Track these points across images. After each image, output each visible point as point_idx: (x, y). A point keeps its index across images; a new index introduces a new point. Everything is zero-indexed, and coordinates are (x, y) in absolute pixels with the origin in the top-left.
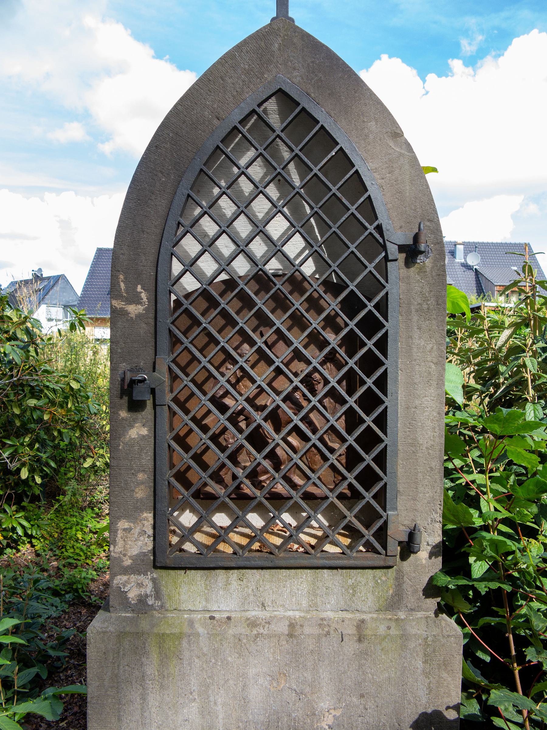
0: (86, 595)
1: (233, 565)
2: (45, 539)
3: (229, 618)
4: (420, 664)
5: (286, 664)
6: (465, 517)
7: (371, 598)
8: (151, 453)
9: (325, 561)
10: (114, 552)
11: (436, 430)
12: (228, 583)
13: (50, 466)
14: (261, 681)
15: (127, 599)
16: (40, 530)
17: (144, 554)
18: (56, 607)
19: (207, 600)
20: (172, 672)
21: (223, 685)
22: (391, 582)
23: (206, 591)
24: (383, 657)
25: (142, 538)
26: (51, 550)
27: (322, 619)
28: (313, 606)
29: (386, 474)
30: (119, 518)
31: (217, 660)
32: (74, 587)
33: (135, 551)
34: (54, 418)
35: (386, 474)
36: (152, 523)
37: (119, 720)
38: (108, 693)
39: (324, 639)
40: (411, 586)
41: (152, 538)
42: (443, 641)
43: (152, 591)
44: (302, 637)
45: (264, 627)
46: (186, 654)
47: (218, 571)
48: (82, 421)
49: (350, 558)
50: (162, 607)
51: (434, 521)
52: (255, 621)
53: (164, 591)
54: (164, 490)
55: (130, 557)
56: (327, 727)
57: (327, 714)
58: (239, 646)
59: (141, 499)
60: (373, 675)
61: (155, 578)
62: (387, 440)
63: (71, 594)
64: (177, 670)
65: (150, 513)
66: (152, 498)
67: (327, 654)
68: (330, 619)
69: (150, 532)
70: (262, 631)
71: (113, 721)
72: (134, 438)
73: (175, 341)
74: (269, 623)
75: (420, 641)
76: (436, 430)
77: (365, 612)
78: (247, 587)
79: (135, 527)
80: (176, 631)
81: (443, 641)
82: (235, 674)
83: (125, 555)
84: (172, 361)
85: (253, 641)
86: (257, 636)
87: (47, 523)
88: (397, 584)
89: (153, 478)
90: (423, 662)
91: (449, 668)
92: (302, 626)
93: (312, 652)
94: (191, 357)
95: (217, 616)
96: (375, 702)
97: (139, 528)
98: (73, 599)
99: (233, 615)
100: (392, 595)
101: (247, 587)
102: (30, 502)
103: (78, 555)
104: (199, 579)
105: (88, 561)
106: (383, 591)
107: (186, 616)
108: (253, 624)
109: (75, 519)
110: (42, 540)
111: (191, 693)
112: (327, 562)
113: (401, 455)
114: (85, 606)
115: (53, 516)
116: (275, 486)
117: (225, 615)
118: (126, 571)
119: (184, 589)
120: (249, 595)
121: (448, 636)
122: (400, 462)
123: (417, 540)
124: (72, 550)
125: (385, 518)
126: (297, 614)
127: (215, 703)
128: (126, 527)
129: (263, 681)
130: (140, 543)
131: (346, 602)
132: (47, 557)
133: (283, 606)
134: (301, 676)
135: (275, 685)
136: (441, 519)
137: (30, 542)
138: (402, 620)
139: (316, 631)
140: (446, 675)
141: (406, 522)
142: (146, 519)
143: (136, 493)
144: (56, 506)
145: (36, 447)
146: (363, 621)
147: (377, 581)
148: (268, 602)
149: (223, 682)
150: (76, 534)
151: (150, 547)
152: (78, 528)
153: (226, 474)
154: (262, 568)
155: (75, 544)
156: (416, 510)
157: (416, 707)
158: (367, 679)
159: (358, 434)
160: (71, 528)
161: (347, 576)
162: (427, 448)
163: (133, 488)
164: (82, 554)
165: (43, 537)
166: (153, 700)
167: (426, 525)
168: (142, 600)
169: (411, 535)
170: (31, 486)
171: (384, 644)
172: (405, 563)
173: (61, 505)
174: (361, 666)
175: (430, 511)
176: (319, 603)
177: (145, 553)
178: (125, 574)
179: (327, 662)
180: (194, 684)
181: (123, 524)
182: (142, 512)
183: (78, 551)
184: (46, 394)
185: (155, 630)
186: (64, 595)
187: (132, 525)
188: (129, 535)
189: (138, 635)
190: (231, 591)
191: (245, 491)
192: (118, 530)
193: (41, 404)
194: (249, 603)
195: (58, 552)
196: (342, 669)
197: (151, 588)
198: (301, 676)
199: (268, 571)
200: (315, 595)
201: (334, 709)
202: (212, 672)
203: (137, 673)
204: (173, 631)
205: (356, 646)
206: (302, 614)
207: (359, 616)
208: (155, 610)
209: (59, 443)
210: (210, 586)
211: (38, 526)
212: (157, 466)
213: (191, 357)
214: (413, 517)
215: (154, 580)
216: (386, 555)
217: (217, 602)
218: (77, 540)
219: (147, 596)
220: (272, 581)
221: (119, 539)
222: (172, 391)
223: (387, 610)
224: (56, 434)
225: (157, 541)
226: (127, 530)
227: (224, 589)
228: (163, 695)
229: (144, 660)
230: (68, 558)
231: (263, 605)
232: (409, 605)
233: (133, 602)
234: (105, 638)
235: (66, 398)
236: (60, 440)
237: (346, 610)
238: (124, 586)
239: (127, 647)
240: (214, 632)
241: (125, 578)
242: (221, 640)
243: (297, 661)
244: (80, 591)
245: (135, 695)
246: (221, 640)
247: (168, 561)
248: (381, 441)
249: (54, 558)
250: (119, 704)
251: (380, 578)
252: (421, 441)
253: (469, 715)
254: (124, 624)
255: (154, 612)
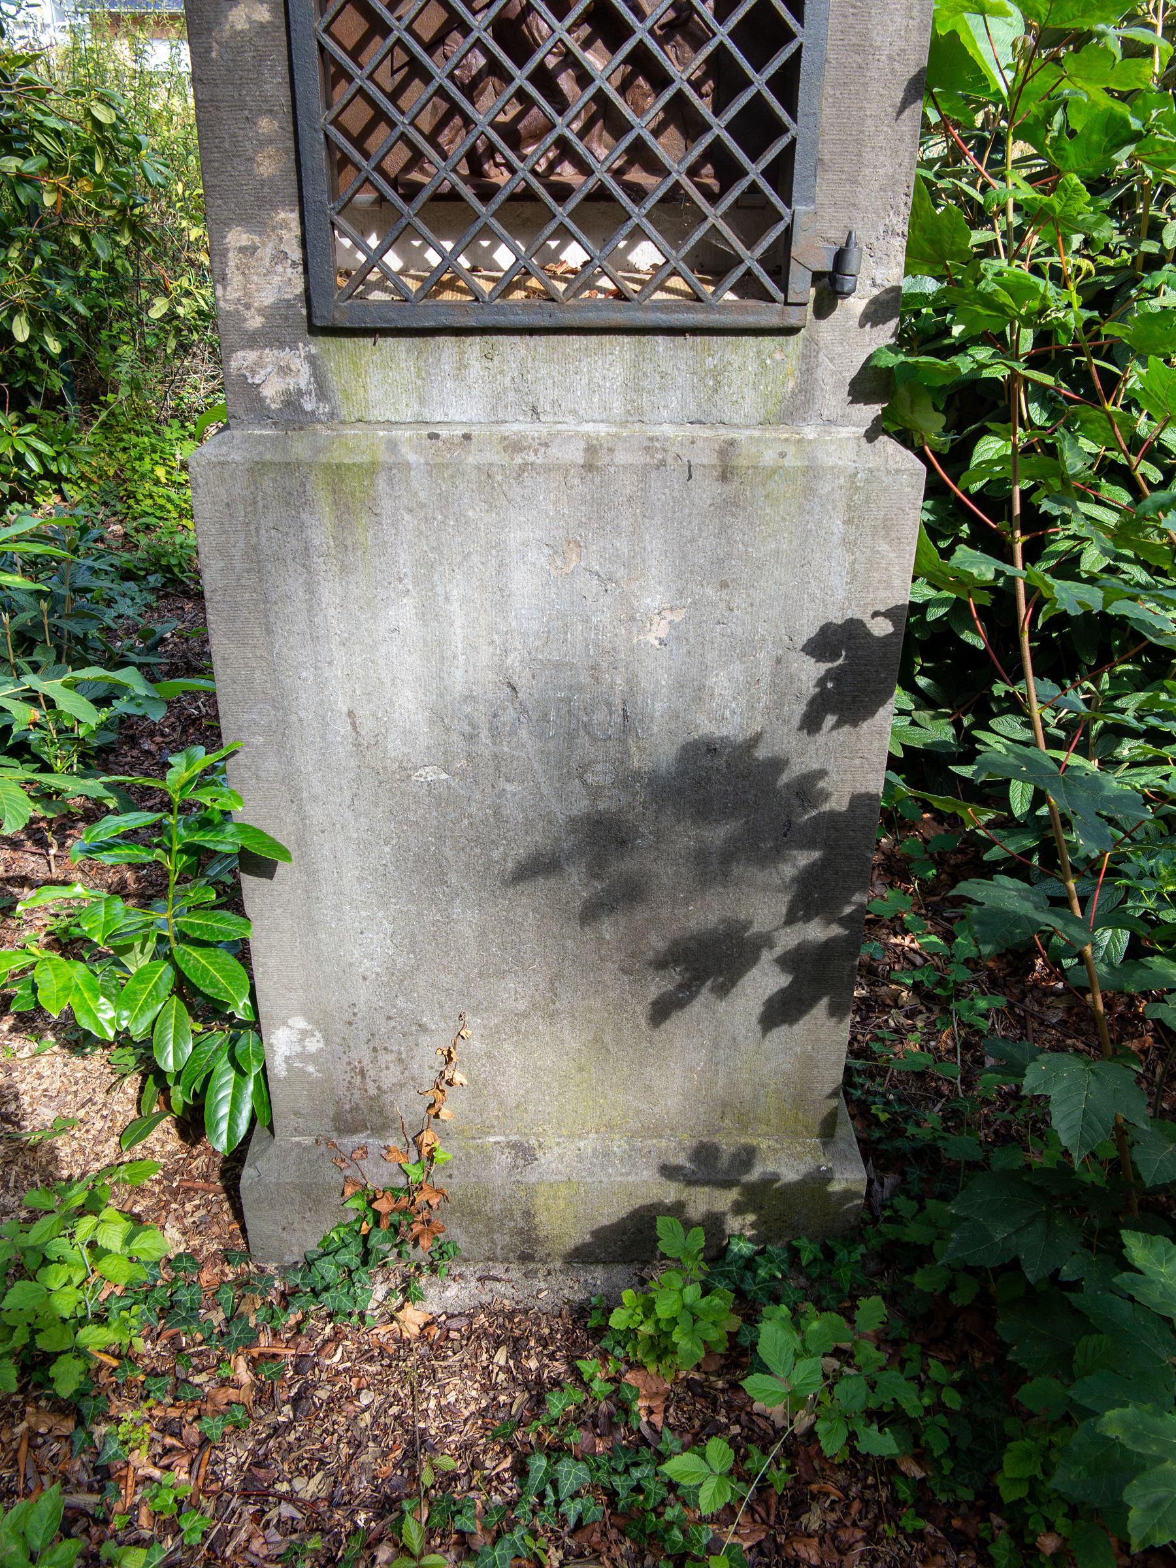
0: (190, 578)
1: (471, 322)
2: (90, 482)
3: (467, 437)
4: (837, 525)
5: (581, 524)
6: (953, 244)
7: (750, 396)
8: (282, 68)
9: (659, 315)
10: (226, 301)
11: (915, 13)
12: (462, 366)
13: (76, 313)
14: (532, 556)
15: (261, 400)
16: (76, 463)
17: (288, 304)
18: (133, 599)
19: (422, 401)
20: (362, 540)
21: (461, 564)
22: (793, 364)
23: (419, 382)
24: (768, 510)
25: (279, 269)
26: (105, 504)
27: (651, 439)
28: (636, 414)
29: (795, 119)
30: (227, 224)
31: (446, 517)
32: (164, 562)
33: (267, 298)
34: (67, 207)
35: (795, 119)
36: (299, 233)
37: (269, 631)
38: (243, 581)
39: (654, 475)
40: (833, 373)
41: (300, 269)
42: (888, 481)
43: (309, 383)
44: (612, 470)
45: (536, 452)
46: (386, 505)
47: (441, 340)
48: (132, 208)
49: (711, 308)
50: (332, 415)
51: (889, 231)
52: (519, 441)
53: (335, 382)
54: (317, 157)
55: (259, 310)
56: (656, 643)
57: (657, 619)
58: (488, 488)
59: (271, 179)
60: (746, 546)
61: (313, 356)
62: (803, 35)
63: (158, 575)
64: (370, 535)
65: (292, 211)
66: (294, 177)
67: (658, 504)
68: (667, 439)
69: (296, 254)
70: (531, 458)
71: (257, 633)
72: (242, 31)
73: (336, 75)
74: (547, 445)
75: (842, 480)
76: (915, 13)
77: (737, 426)
78: (502, 372)
79: (264, 244)
80: (365, 459)
81: (888, 481)
82: (483, 543)
83: (248, 306)
84: (331, 123)
85: (516, 479)
86: (523, 468)
87: (88, 449)
88: (804, 367)
89: (291, 129)
90: (844, 522)
91: (893, 535)
92: (611, 450)
93: (630, 499)
94: (372, 112)
95: (443, 432)
96: (749, 596)
97: (271, 245)
98: (164, 585)
99: (475, 431)
100: (793, 392)
101: (502, 372)
102: (46, 407)
103: (162, 508)
104: (403, 356)
105: (185, 522)
106: (774, 381)
107: (381, 433)
108: (514, 446)
109: (146, 439)
110: (83, 485)
111: (400, 580)
112: (663, 316)
113: (831, 74)
114: (189, 598)
115: (99, 438)
116: (558, 170)
117: (459, 431)
118: (253, 340)
119: (374, 378)
120: (505, 390)
121: (897, 471)
122: (829, 90)
123: (851, 268)
124: (150, 502)
125: (787, 220)
126: (603, 429)
127: (447, 599)
128: (244, 244)
129: (538, 557)
130: (276, 280)
131: (699, 405)
132: (100, 517)
133: (574, 412)
134: (609, 546)
135: (559, 563)
136: (906, 229)
137: (59, 491)
138: (810, 441)
139: (639, 459)
140: (887, 547)
141: (832, 234)
142: (285, 225)
143: (259, 165)
144: (103, 415)
145: (36, 265)
146: (732, 443)
147: (764, 361)
148: (544, 405)
149: (459, 558)
150: (153, 471)
151: (299, 289)
152: (156, 457)
153: (451, 142)
154: (532, 331)
155: (155, 489)
156: (854, 205)
157: (825, 606)
158: (735, 553)
159: (740, 17)
160: (141, 459)
161: (703, 350)
162: (890, 58)
163: (250, 153)
164: (169, 506)
165: (83, 477)
166: (329, 592)
167: (873, 240)
168: (292, 401)
169: (840, 258)
170: (41, 372)
171: (771, 486)
172: (823, 323)
173: (112, 414)
174: (724, 528)
175: (885, 209)
176: (647, 407)
177: (288, 301)
178: (252, 348)
179: (658, 520)
180: (405, 561)
181: (237, 237)
182: (274, 208)
183: (161, 501)
184: (40, 144)
185: (323, 458)
186: (145, 577)
187: (256, 238)
188: (253, 263)
189: (289, 467)
190: (470, 382)
191: (494, 180)
192: (227, 250)
193: (32, 169)
194: (506, 407)
195: (119, 507)
196: (688, 533)
197: (307, 376)
198: (609, 546)
199: (544, 338)
200: (639, 390)
201: (671, 609)
202: (438, 539)
203: (295, 543)
204: (359, 459)
205: (718, 488)
206: (613, 430)
207: (724, 433)
208: (319, 421)
209: (87, 273)
210: (428, 372)
211: (71, 457)
212: (298, 97)
213: (372, 112)
214: (846, 221)
215: (311, 360)
216: (786, 303)
217: (442, 404)
218: (157, 482)
219: (300, 393)
220: (551, 361)
221: (231, 271)
222: (329, 106)
223: (781, 421)
224: (76, 241)
225: (311, 271)
226: (248, 251)
227: (456, 378)
228: (348, 583)
229: (305, 516)
230: (141, 516)
231: (534, 409)
232: (826, 413)
233: (273, 406)
234: (226, 476)
235: (88, 151)
236: (90, 267)
237: (700, 422)
238: (254, 372)
239: (270, 491)
240: (439, 460)
241: (252, 356)
242: (453, 476)
243: (602, 518)
244: (176, 570)
245: (292, 584)
246: (453, 476)
247: (337, 315)
248: (792, 36)
249: (113, 519)
250: (266, 602)
251: (770, 356)
252: (879, 39)
253: (934, 743)
254: (261, 448)
255: (319, 427)
